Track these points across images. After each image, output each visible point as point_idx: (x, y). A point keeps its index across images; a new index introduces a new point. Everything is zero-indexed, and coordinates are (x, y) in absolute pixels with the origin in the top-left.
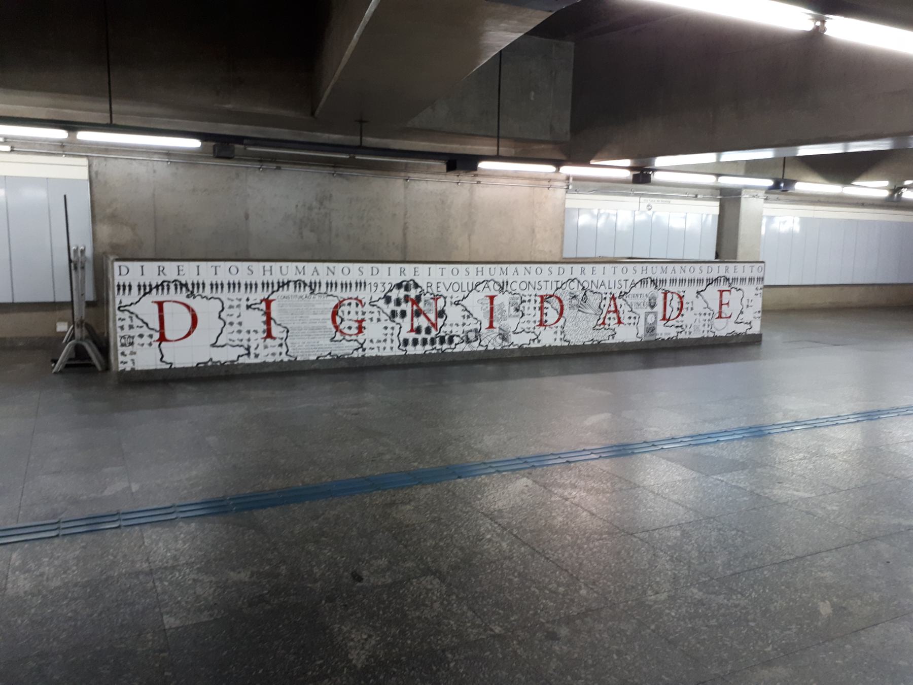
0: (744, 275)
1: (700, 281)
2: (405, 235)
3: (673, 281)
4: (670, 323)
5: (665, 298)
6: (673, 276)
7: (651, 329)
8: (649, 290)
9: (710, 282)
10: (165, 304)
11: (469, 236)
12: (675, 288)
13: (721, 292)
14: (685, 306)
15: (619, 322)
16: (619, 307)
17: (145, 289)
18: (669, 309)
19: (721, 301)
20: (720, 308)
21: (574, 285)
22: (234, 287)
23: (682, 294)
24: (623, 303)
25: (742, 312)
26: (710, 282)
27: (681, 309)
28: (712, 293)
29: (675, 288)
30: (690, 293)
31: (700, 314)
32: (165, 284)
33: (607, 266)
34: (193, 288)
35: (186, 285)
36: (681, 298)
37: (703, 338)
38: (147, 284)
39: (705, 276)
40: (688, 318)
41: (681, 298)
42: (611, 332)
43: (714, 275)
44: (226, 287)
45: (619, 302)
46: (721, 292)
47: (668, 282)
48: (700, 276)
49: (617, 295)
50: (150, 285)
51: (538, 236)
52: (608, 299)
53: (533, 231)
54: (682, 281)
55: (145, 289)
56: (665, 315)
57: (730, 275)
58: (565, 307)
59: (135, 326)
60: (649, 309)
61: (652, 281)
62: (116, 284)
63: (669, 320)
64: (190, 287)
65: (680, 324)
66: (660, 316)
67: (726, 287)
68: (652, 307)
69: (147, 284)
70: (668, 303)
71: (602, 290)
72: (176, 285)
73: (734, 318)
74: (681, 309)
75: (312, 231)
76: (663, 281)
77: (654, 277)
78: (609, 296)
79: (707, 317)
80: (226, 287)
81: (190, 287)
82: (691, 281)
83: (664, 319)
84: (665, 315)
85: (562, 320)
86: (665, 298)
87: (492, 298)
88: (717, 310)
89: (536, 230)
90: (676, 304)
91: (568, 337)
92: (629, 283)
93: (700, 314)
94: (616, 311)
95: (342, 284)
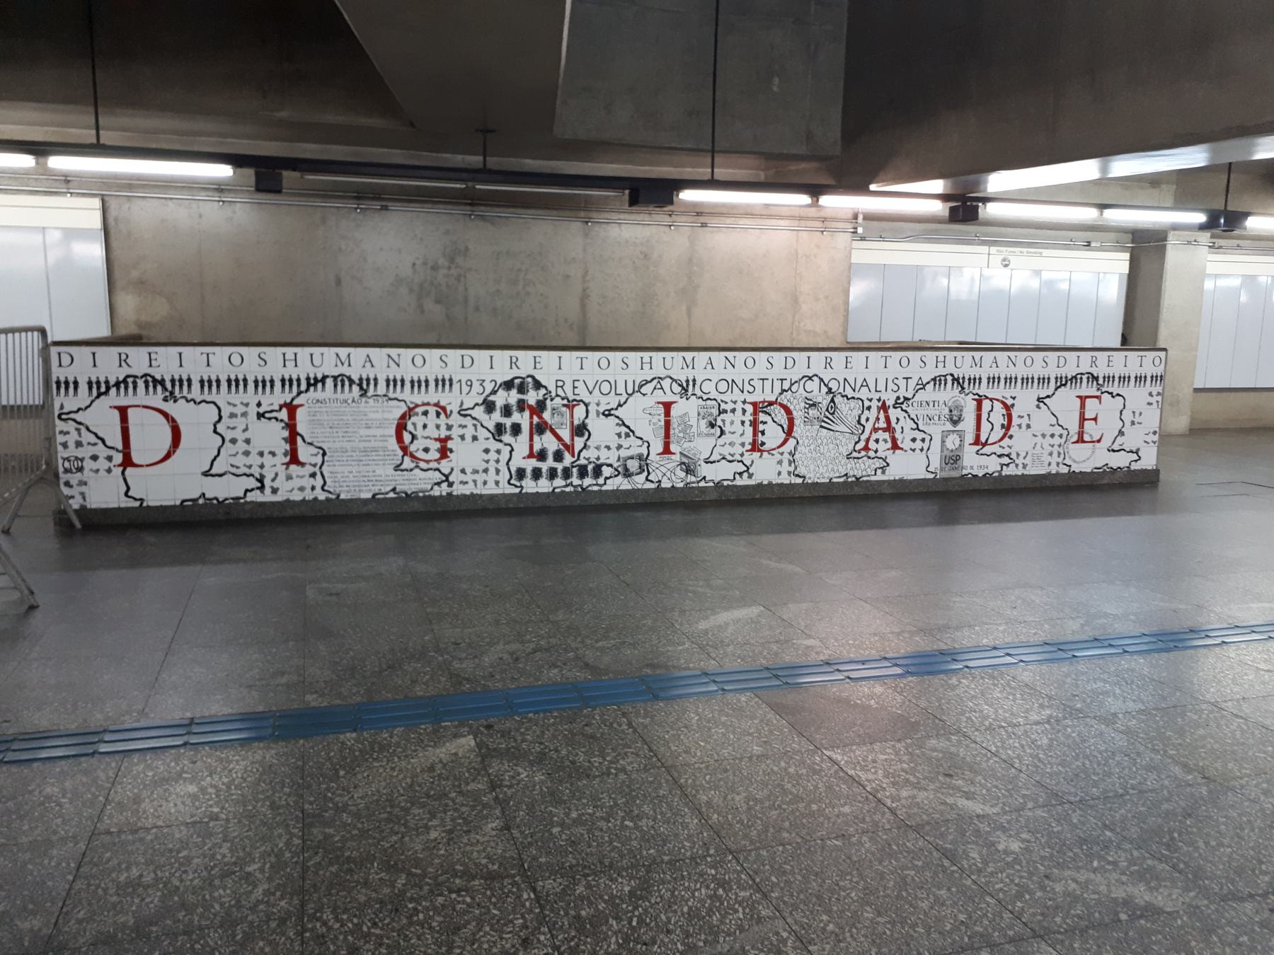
1: (1043, 381)
3: (992, 380)
4: (987, 450)
6: (994, 372)
7: (953, 459)
8: (949, 394)
9: (1062, 382)
12: (997, 392)
14: (1015, 421)
15: (895, 446)
16: (893, 421)
18: (985, 426)
20: (1081, 426)
23: (1009, 402)
25: (1121, 433)
26: (1062, 382)
27: (1007, 427)
30: (1024, 400)
31: (1044, 436)
35: (1096, 379)
40: (1021, 441)
41: (1008, 408)
43: (1070, 371)
45: (893, 413)
46: (1083, 399)
49: (890, 403)
51: (804, 307)
54: (1010, 380)
56: (978, 437)
57: (1100, 371)
60: (949, 426)
61: (956, 380)
65: (1006, 451)
66: (970, 438)
70: (984, 416)
74: (1007, 427)
75: (438, 302)
76: (974, 381)
79: (1057, 440)
81: (1101, 381)
82: (1026, 381)
83: (977, 441)
84: (978, 437)
85: (792, 442)
87: (667, 406)
88: (1074, 428)
89: (801, 299)
90: (998, 417)
93: (1044, 436)
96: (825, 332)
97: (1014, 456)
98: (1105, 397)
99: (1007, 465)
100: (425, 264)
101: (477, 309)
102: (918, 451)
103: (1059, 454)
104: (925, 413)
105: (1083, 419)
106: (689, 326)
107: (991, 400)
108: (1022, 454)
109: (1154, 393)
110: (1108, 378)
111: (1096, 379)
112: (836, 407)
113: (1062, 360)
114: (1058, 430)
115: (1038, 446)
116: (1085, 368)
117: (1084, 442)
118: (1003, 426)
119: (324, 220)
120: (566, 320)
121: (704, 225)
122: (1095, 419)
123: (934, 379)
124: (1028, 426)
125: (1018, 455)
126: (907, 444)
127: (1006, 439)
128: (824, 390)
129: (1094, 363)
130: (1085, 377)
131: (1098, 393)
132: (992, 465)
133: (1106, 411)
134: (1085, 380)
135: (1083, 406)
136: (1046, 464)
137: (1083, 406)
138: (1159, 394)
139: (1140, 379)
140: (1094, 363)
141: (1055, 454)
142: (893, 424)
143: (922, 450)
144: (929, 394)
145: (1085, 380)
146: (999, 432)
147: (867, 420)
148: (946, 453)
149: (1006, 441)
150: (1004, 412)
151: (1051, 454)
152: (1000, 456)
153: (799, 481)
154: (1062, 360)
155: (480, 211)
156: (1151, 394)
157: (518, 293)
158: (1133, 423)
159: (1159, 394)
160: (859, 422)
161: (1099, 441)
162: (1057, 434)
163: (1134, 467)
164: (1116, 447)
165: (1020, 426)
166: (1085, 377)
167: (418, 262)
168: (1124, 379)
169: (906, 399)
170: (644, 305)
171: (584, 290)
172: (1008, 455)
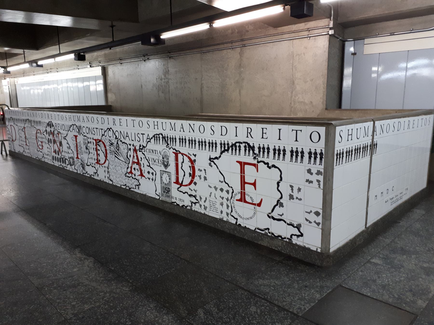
0: (281, 145)
1: (213, 145)
2: (202, 91)
3: (182, 140)
4: (183, 189)
5: (177, 159)
6: (183, 135)
7: (167, 190)
8: (161, 147)
9: (226, 148)
10: (246, 166)
11: (240, 91)
12: (185, 149)
13: (242, 165)
14: (197, 173)
15: (142, 175)
16: (140, 159)
17: (225, 147)
18: (181, 173)
19: (243, 178)
20: (243, 188)
21: (111, 133)
22: (315, 158)
23: (193, 158)
24: (143, 156)
25: (279, 203)
26: (226, 148)
27: (193, 175)
28: (229, 162)
29: (185, 149)
30: (202, 157)
31: (216, 188)
32: (238, 144)
33: (284, 128)
34: (259, 151)
35: (253, 148)
36: (192, 162)
37: (221, 220)
38: (226, 143)
39: (218, 139)
40: (201, 189)
41: (192, 162)
42: (136, 183)
43: (231, 139)
44: (306, 156)
45: (140, 154)
46: (242, 165)
47: (178, 141)
48: (213, 139)
49: (137, 148)
50: (228, 144)
51: (298, 88)
52: (132, 150)
53: (293, 83)
54: (192, 142)
55: (225, 147)
56: (177, 178)
57: (256, 141)
58: (108, 152)
59: (295, 197)
60: (163, 168)
61: (164, 138)
62: (336, 153)
63: (181, 185)
64: (256, 151)
65: (193, 193)
66: (174, 179)
67: (250, 159)
68: (166, 166)
69: (226, 143)
70: (180, 165)
71: (127, 141)
72: (245, 147)
73: (266, 207)
74: (193, 175)
75: (163, 92)
76: (173, 139)
77: (165, 133)
78: (132, 148)
79: (224, 194)
80: (306, 156)
81: (256, 151)
82: (202, 143)
83: (177, 182)
84: (177, 178)
85: (107, 161)
86: (177, 159)
87: (76, 136)
88: (237, 188)
89: (296, 82)
90: (187, 165)
91: (111, 178)
92: (145, 137)
93: (216, 188)
94: (138, 163)
95: (274, 150)
96: (311, 102)
97: (198, 198)
98: (261, 165)
99: (195, 203)
100: (159, 78)
101: (172, 95)
102: (151, 180)
103: (228, 206)
104: (153, 157)
105: (243, 183)
106: (240, 100)
107: (182, 154)
108: (203, 199)
109: (314, 171)
110: (263, 150)
111: (253, 148)
112: (119, 147)
113: (224, 129)
114: (225, 187)
115: (213, 195)
116: (242, 137)
117: (245, 202)
118: (190, 174)
119: (138, 65)
120: (196, 99)
121: (244, 46)
122: (254, 184)
123: (154, 136)
124: (205, 179)
125: (201, 198)
126: (146, 174)
127: (193, 184)
128: (115, 137)
129: (249, 133)
130: (242, 146)
131: (255, 162)
132: (186, 201)
133: (264, 179)
134: (243, 148)
135: (242, 171)
136: (219, 211)
137: (242, 171)
138: (319, 173)
139: (296, 154)
140: (249, 133)
141: (225, 206)
142: (140, 161)
143: (153, 180)
144: (152, 146)
145: (243, 148)
146: (187, 180)
147: (130, 156)
148: (163, 185)
149: (192, 186)
150: (190, 164)
151: (222, 204)
152: (190, 195)
153: (111, 183)
154: (224, 129)
155: (192, 51)
156: (309, 171)
157: (182, 87)
158: (291, 197)
159: (319, 173)
160: (127, 157)
161: (259, 205)
162: (225, 189)
163: (295, 240)
164: (275, 214)
165: (200, 176)
166: (242, 146)
167: (157, 78)
168: (279, 152)
169: (144, 147)
170: (222, 90)
171: (202, 84)
172: (195, 197)
